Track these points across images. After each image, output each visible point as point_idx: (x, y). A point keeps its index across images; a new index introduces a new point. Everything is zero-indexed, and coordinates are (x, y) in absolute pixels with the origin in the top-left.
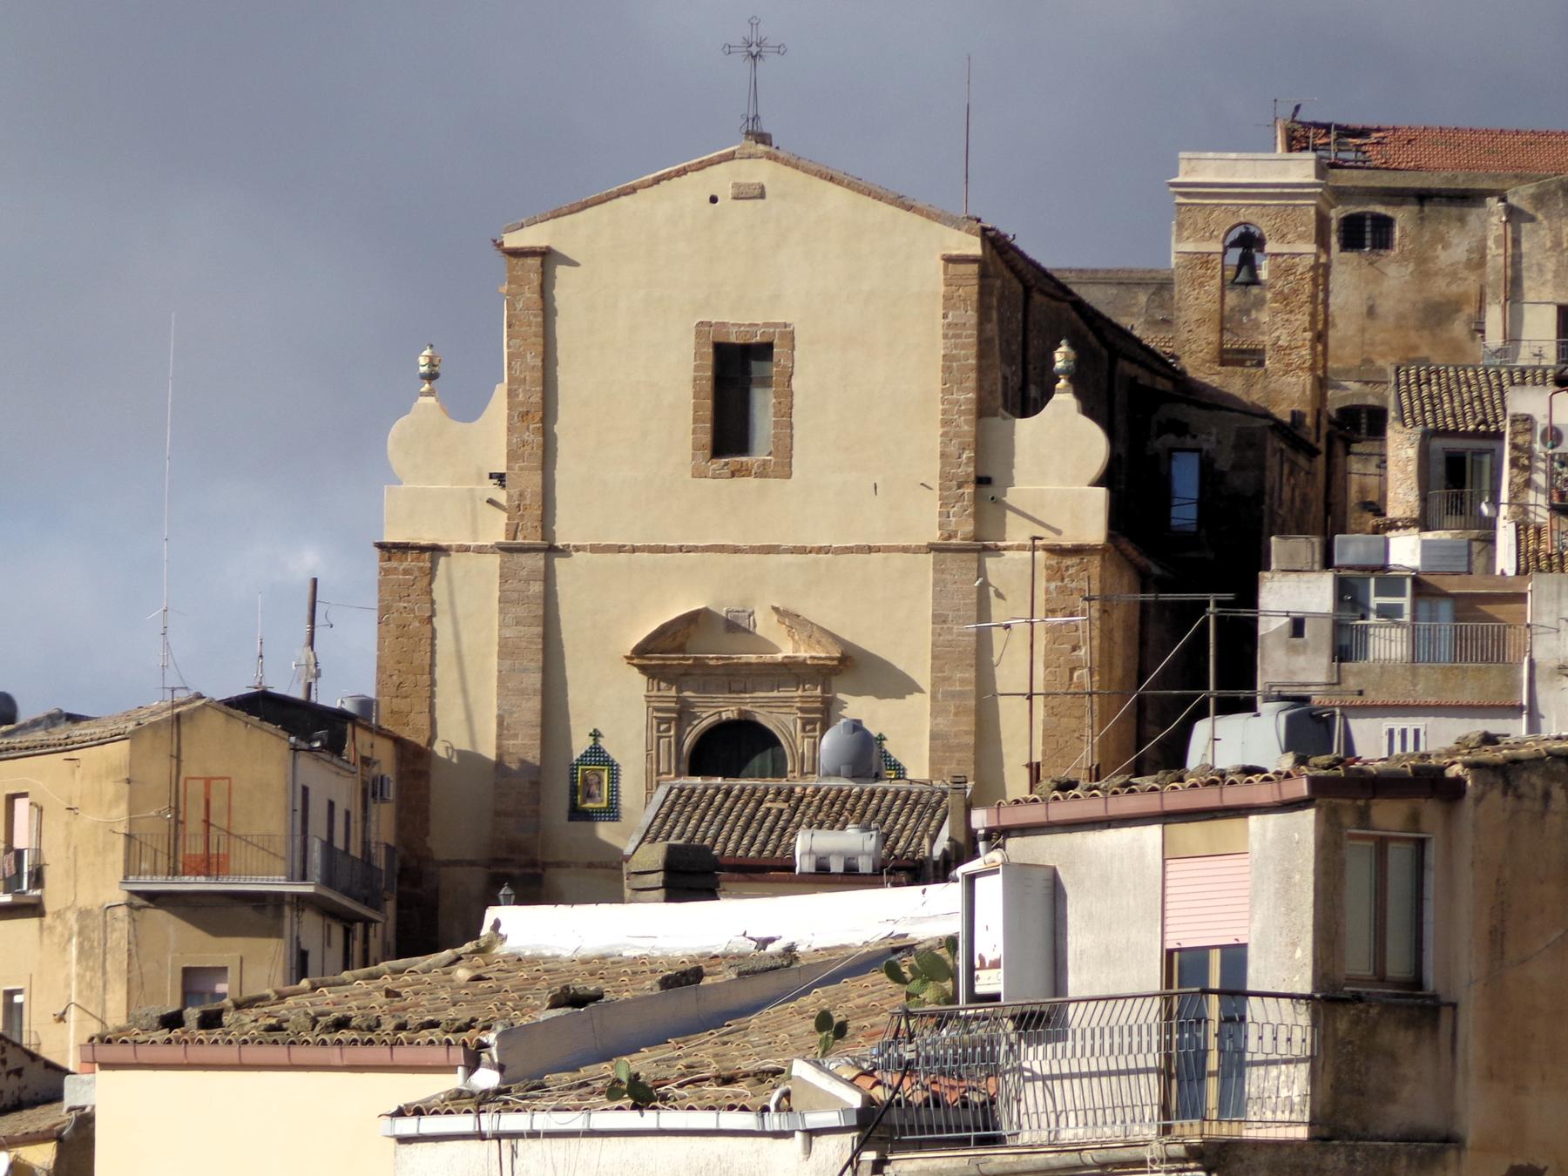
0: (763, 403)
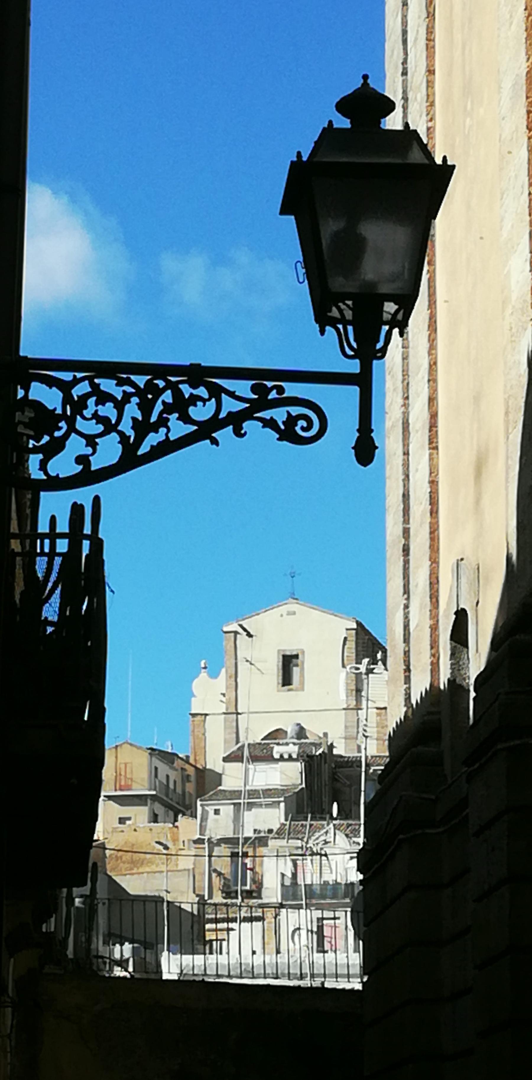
0: (296, 670)
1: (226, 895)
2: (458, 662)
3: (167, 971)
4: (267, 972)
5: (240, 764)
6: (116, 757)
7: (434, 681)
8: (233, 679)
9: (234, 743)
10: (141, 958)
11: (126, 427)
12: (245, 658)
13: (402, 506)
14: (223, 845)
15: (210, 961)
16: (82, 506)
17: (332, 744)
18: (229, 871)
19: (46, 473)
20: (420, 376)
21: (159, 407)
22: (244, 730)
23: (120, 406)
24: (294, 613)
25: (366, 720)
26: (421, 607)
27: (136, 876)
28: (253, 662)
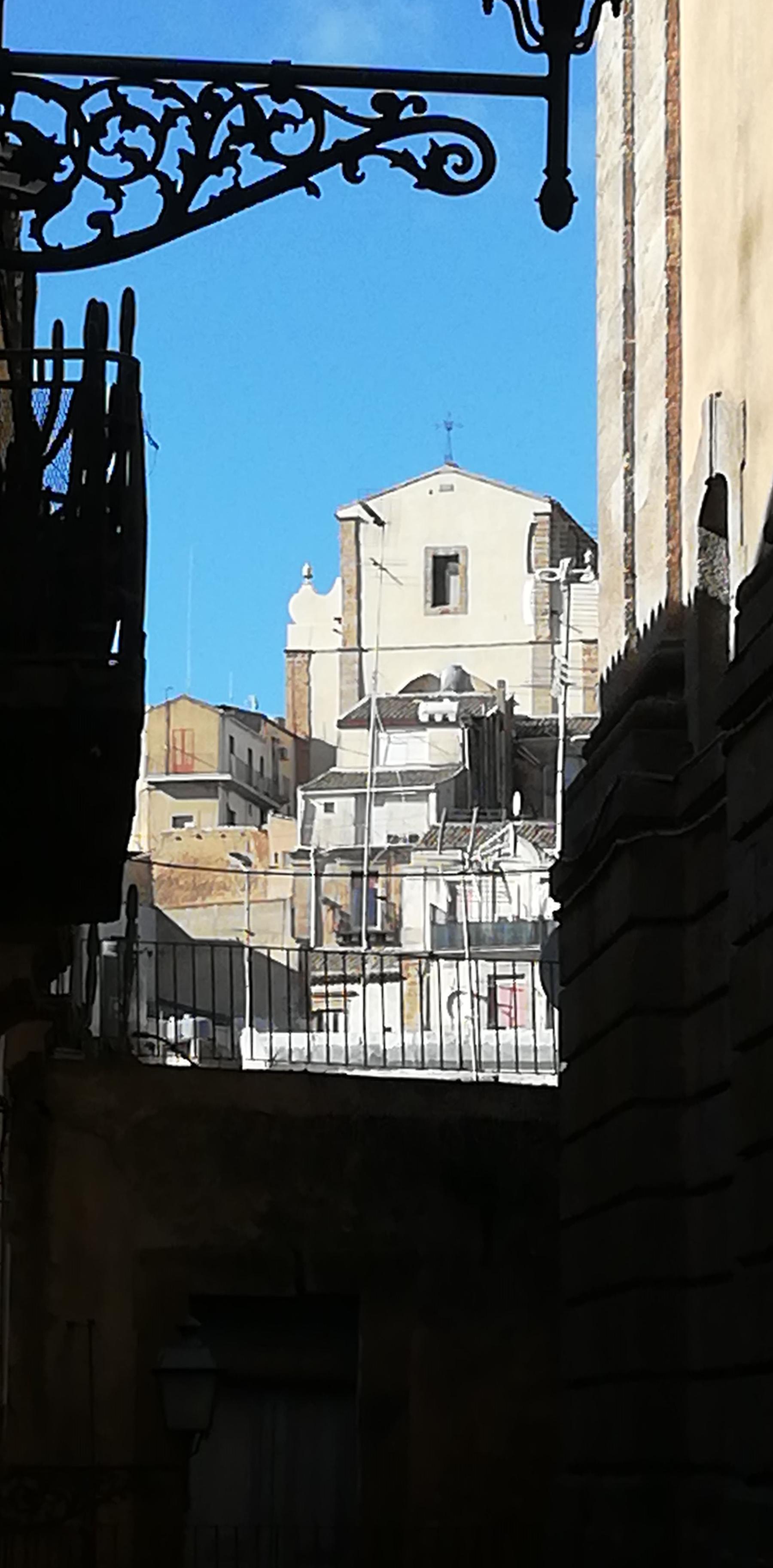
0: (454, 581)
1: (344, 940)
2: (712, 561)
3: (249, 1057)
4: (407, 1059)
5: (366, 731)
6: (168, 720)
7: (674, 591)
8: (354, 594)
9: (357, 698)
10: (209, 1039)
11: (170, 165)
12: (372, 559)
13: (622, 309)
14: (339, 861)
15: (317, 1043)
16: (104, 306)
17: (512, 699)
18: (348, 902)
19: (41, 242)
20: (652, 94)
21: (222, 133)
22: (371, 675)
23: (159, 132)
24: (452, 488)
25: (566, 657)
26: (653, 471)
27: (200, 909)
28: (384, 566)
